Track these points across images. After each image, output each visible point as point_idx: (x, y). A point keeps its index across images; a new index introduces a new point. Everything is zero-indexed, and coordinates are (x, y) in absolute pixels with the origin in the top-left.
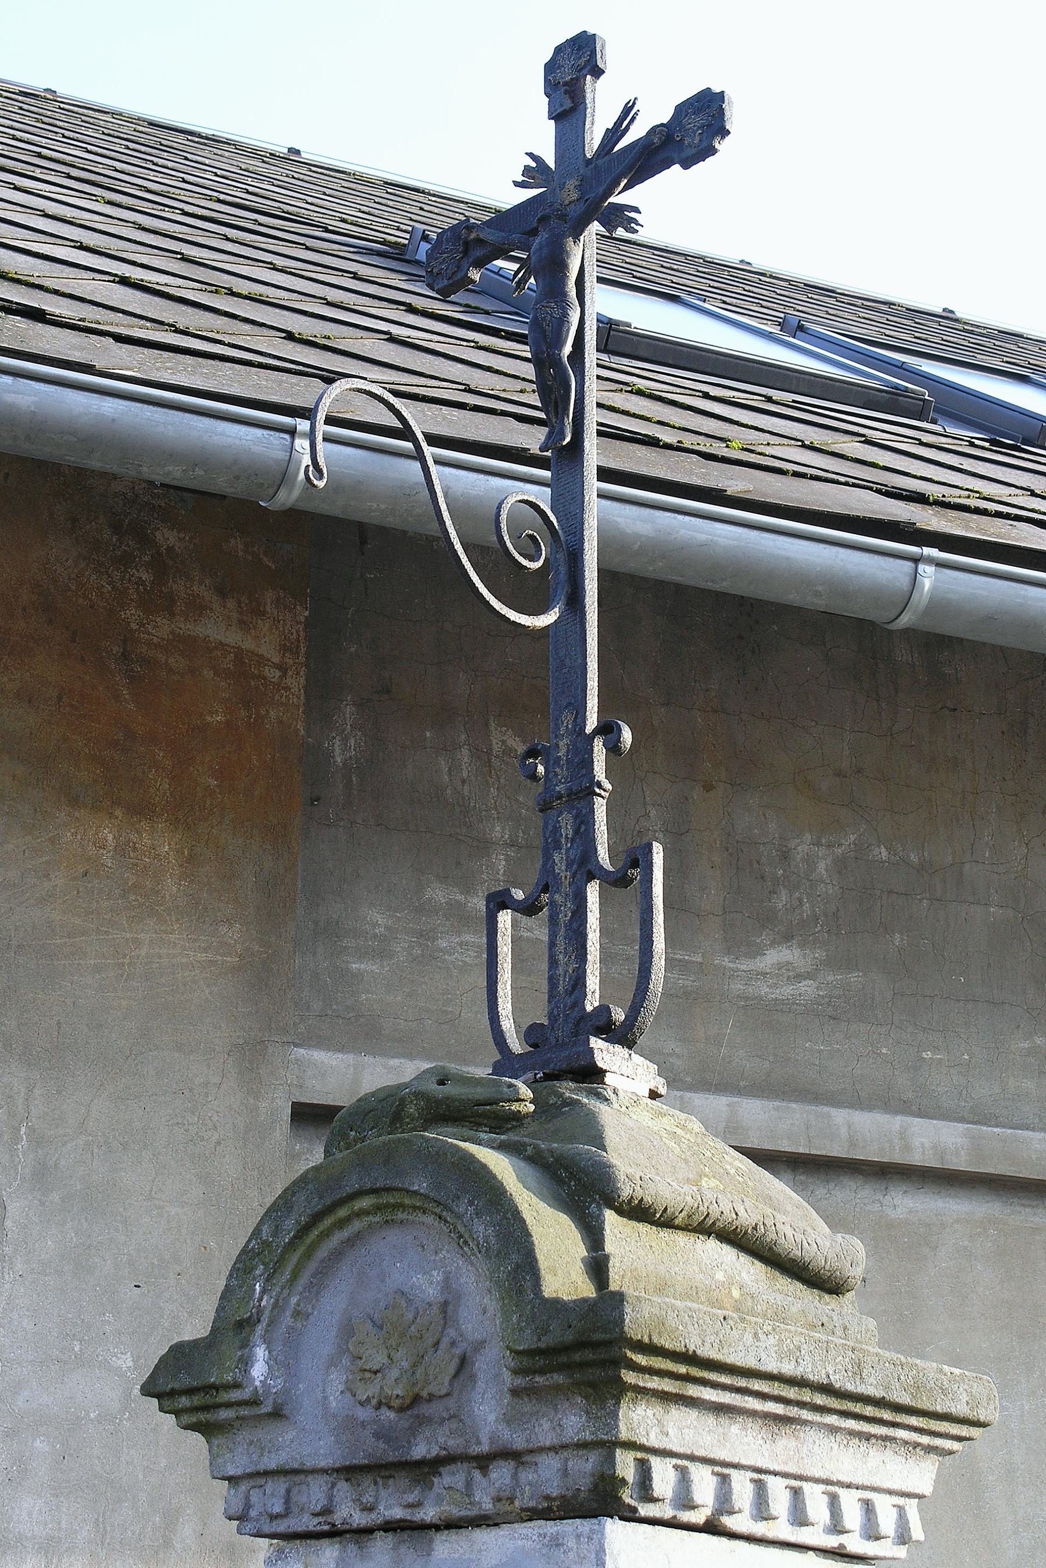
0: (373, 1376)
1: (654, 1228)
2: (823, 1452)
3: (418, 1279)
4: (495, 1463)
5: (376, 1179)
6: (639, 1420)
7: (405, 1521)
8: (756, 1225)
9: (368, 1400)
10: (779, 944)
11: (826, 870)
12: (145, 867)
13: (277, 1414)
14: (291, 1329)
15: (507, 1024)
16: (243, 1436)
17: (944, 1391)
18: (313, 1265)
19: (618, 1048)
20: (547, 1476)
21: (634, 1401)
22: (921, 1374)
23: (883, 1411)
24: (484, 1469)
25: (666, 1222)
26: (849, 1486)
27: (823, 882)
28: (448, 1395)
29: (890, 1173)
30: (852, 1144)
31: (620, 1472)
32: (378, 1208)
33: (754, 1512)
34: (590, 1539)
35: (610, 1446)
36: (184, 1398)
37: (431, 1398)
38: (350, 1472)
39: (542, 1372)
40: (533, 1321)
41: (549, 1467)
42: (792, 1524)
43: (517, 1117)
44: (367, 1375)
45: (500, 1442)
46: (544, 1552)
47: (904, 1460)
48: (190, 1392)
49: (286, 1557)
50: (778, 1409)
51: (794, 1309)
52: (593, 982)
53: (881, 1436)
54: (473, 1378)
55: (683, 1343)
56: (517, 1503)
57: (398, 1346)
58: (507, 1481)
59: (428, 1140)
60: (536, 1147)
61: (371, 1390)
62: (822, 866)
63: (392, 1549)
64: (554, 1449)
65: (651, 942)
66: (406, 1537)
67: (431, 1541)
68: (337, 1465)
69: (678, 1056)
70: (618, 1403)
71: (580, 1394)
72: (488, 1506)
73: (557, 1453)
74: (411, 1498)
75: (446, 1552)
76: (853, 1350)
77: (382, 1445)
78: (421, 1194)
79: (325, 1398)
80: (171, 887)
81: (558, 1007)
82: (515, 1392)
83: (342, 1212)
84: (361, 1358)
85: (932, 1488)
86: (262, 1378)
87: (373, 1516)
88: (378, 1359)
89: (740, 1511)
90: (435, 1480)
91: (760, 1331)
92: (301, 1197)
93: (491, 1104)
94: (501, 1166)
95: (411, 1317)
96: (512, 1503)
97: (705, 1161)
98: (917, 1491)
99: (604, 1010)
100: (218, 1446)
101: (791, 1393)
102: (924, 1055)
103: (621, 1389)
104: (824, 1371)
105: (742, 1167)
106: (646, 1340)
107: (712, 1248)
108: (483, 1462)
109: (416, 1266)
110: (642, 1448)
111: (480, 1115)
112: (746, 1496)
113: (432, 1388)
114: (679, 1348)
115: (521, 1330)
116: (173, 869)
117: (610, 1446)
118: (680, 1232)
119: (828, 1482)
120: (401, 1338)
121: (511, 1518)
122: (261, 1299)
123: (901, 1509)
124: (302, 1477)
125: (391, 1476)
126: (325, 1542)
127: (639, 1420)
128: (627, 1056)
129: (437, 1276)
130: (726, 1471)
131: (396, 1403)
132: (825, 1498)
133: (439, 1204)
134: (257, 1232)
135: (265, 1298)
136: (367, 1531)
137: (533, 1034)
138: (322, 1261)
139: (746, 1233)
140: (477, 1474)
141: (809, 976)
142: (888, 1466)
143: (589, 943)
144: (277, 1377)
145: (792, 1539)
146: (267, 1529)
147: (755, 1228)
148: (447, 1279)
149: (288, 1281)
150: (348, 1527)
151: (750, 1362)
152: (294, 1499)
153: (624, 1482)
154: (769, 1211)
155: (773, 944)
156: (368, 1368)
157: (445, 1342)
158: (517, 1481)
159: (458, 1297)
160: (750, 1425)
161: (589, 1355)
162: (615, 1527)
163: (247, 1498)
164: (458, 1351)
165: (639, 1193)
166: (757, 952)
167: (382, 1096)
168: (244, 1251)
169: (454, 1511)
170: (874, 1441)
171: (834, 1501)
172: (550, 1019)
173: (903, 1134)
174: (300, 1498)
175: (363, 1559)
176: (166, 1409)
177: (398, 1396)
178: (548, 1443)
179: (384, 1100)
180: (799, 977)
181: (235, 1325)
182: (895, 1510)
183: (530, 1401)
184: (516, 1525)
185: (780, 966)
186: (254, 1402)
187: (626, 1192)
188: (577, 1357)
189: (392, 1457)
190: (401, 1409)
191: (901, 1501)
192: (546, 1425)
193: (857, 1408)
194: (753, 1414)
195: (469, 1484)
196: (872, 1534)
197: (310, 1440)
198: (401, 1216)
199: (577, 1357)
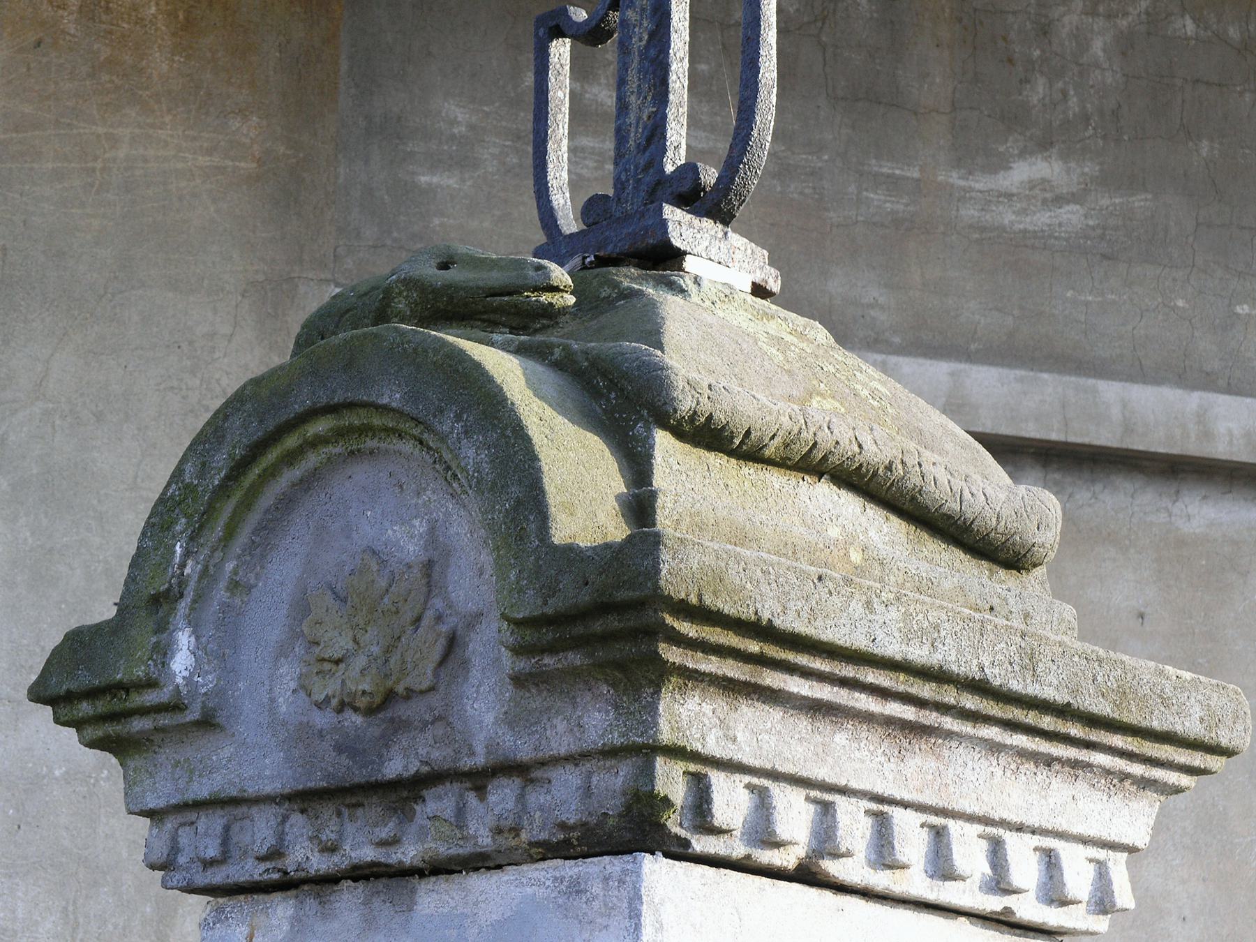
0: (334, 668)
1: (733, 461)
2: (976, 776)
3: (396, 532)
4: (495, 782)
5: (334, 391)
6: (689, 716)
7: (378, 864)
8: (891, 463)
9: (327, 700)
10: (1032, 153)
11: (1104, 50)
12: (123, 36)
13: (207, 723)
14: (226, 608)
15: (561, 199)
16: (167, 755)
17: (1164, 701)
18: (253, 519)
19: (707, 223)
20: (563, 798)
21: (682, 690)
22: (1130, 676)
23: (1069, 724)
24: (481, 790)
25: (749, 452)
26: (1020, 828)
27: (1097, 66)
28: (432, 689)
29: (1183, 471)
30: (1128, 429)
31: (661, 788)
32: (340, 434)
33: (873, 857)
34: (621, 882)
35: (648, 751)
36: (85, 704)
37: (410, 694)
38: (304, 799)
39: (552, 649)
40: (537, 578)
41: (566, 781)
42: (932, 877)
43: (550, 314)
44: (327, 666)
45: (500, 752)
46: (560, 901)
47: (1105, 798)
48: (92, 694)
49: (227, 918)
50: (908, 713)
51: (947, 585)
52: (677, 134)
53: (1069, 760)
54: (465, 664)
55: (752, 609)
56: (524, 836)
57: (367, 623)
58: (510, 805)
59: (403, 333)
60: (566, 348)
61: (329, 687)
62: (1097, 46)
63: (363, 904)
64: (573, 759)
65: (756, 69)
66: (381, 887)
67: (413, 891)
68: (287, 791)
69: (882, 308)
70: (657, 692)
71: (606, 681)
72: (485, 841)
73: (576, 765)
74: (384, 833)
75: (432, 905)
76: (1023, 635)
77: (345, 761)
78: (393, 410)
79: (273, 700)
80: (160, 63)
81: (626, 170)
82: (519, 681)
83: (291, 441)
84: (318, 644)
85: (1147, 839)
86: (186, 674)
87: (336, 858)
88: (340, 644)
89: (848, 854)
90: (418, 808)
91: (876, 600)
92: (236, 422)
93: (510, 294)
94: (502, 365)
95: (383, 583)
96: (518, 835)
97: (822, 377)
98: (1125, 841)
99: (689, 169)
100: (135, 771)
101: (926, 690)
102: (1239, 309)
103: (661, 672)
104: (975, 662)
105: (883, 390)
106: (694, 600)
107: (824, 493)
108: (479, 780)
109: (392, 514)
110: (695, 757)
111: (495, 310)
112: (858, 834)
113: (409, 682)
114: (747, 614)
115: (521, 591)
116: (163, 39)
117: (648, 751)
118: (774, 470)
119: (986, 821)
120: (371, 613)
121: (517, 856)
122: (183, 565)
123: (1101, 866)
124: (245, 809)
125: (360, 805)
126: (277, 897)
127: (689, 716)
128: (720, 235)
129: (420, 526)
130: (828, 797)
131: (362, 702)
132: (984, 844)
133: (418, 422)
134: (177, 474)
135: (190, 563)
136: (329, 881)
137: (593, 210)
138: (267, 511)
139: (875, 474)
140: (472, 798)
141: (1074, 198)
142: (1080, 804)
143: (673, 77)
144: (207, 673)
145: (931, 896)
146: (201, 879)
147: (889, 468)
148: (432, 530)
149: (220, 540)
150: (303, 874)
151: (859, 641)
152: (235, 840)
153: (667, 802)
154: (912, 445)
155: (1023, 154)
156: (327, 656)
157: (429, 614)
158: (524, 806)
159: (447, 554)
160: (864, 735)
161: (613, 623)
162: (656, 867)
163: (174, 839)
164: (444, 629)
165: (706, 407)
166: (1000, 164)
167: (364, 289)
168: (162, 501)
169: (442, 850)
170: (1058, 767)
171: (996, 850)
172: (615, 186)
173: (1202, 416)
174: (241, 837)
175: (325, 917)
176: (62, 719)
177: (364, 692)
178: (563, 751)
179: (366, 294)
180: (1059, 200)
181: (151, 599)
182: (1092, 867)
183: (540, 692)
184: (525, 867)
185: (1032, 185)
186: (175, 706)
187: (685, 404)
188: (597, 626)
189: (359, 776)
190: (370, 711)
191: (1101, 854)
192: (561, 726)
193: (1030, 718)
194: (868, 718)
195: (461, 812)
196: (1055, 896)
197: (252, 758)
198: (371, 443)
199: (597, 626)
